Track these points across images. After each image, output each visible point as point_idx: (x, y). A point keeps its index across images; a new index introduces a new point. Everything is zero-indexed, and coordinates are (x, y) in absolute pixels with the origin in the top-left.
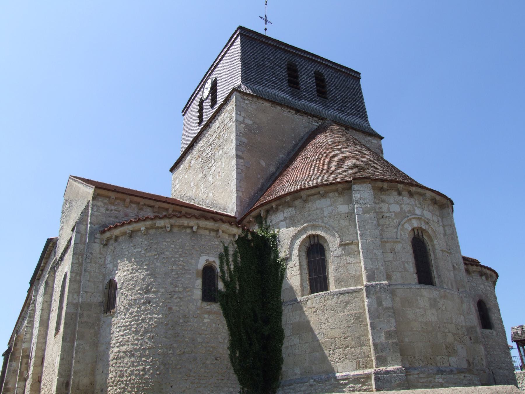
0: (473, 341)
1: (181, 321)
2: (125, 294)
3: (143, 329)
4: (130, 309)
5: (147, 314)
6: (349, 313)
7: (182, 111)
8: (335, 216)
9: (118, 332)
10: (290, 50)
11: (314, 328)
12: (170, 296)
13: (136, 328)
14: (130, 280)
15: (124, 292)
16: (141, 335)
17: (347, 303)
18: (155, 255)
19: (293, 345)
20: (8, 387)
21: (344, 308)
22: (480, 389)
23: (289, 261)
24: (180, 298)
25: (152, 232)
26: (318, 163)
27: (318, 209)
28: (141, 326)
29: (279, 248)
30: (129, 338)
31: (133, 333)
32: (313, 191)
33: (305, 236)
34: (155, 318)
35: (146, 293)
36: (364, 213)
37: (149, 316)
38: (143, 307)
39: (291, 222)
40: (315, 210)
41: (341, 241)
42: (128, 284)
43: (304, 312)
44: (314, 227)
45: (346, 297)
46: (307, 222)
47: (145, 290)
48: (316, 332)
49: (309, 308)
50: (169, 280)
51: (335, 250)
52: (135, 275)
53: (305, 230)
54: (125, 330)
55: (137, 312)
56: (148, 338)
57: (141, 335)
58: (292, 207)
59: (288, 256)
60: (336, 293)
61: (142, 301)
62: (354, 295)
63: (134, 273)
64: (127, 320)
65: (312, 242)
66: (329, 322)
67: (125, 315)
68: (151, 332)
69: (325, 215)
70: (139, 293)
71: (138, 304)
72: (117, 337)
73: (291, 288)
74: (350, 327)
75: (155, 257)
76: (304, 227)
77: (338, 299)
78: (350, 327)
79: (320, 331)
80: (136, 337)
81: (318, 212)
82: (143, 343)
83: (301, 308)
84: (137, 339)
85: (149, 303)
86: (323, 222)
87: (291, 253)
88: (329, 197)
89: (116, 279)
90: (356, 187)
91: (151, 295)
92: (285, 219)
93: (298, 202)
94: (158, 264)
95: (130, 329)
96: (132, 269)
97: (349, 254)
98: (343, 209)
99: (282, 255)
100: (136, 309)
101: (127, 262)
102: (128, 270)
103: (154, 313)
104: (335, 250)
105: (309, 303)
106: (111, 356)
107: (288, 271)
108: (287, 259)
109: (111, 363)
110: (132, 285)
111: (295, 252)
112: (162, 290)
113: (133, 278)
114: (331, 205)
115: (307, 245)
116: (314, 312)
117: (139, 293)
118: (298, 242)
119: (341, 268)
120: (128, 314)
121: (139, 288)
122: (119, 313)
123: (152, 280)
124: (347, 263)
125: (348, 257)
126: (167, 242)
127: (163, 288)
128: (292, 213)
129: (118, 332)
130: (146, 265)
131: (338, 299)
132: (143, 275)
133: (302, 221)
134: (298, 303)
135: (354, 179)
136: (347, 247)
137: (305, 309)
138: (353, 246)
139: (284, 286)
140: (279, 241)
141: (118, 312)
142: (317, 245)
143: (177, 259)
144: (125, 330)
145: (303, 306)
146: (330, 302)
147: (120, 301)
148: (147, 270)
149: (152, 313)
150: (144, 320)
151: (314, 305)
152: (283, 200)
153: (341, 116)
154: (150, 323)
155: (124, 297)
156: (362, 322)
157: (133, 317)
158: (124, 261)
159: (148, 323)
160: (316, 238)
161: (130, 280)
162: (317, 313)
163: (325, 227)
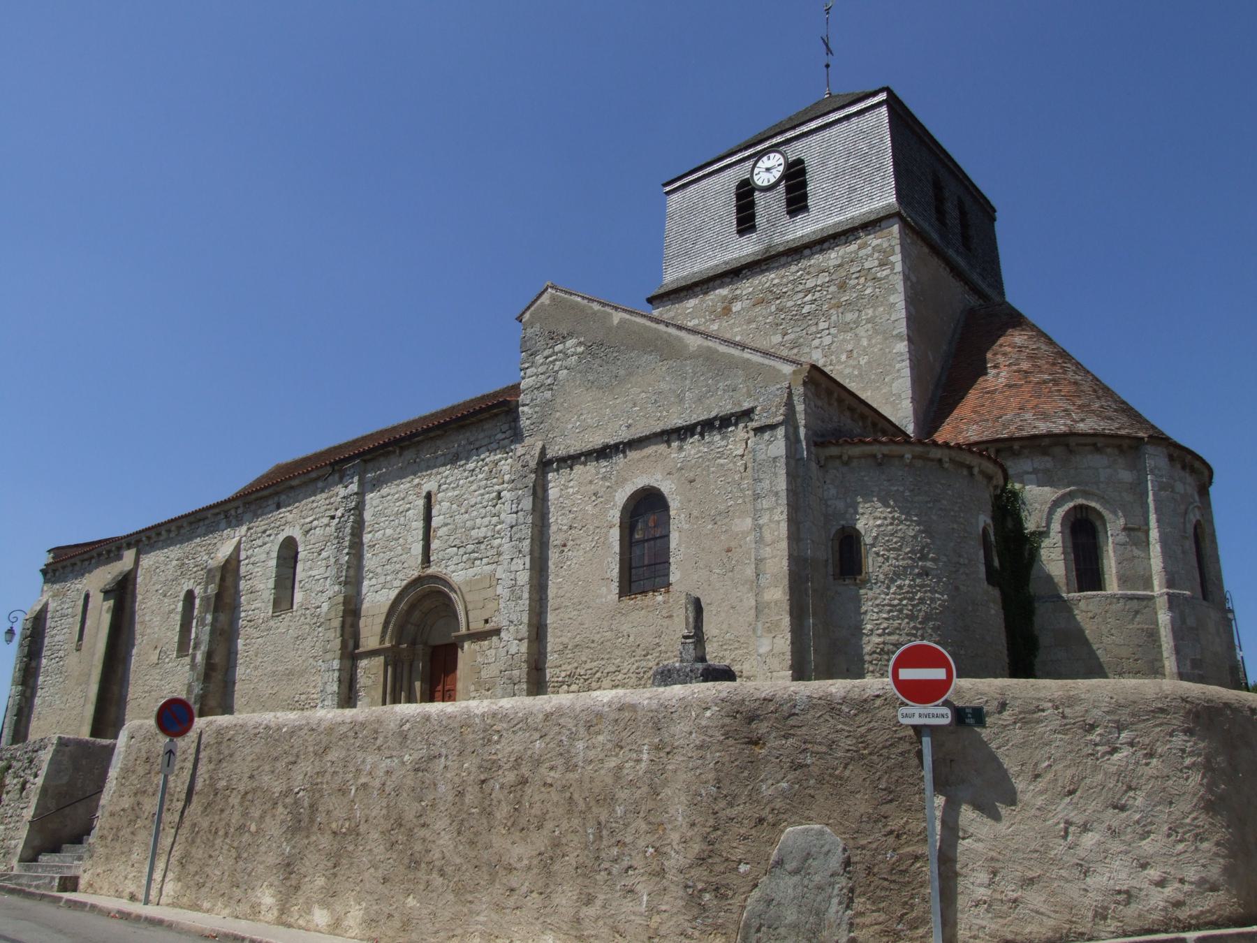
1: (970, 608)
2: (884, 555)
3: (922, 614)
4: (896, 581)
5: (926, 592)
6: (1138, 627)
7: (665, 182)
9: (877, 613)
10: (934, 148)
11: (1091, 641)
12: (954, 569)
13: (910, 610)
14: (892, 535)
15: (882, 553)
16: (920, 623)
17: (1137, 612)
18: (927, 502)
20: (212, 661)
21: (1133, 620)
23: (1045, 538)
24: (967, 574)
25: (919, 463)
26: (1060, 391)
28: (919, 608)
29: (1024, 514)
30: (900, 624)
31: (907, 618)
32: (1089, 440)
33: (1071, 504)
34: (939, 599)
35: (920, 559)
36: (1159, 490)
37: (929, 594)
38: (918, 581)
39: (1046, 479)
40: (1085, 469)
41: (1126, 524)
42: (888, 541)
43: (1074, 616)
44: (1086, 494)
45: (1135, 605)
46: (1073, 484)
47: (918, 555)
48: (1095, 647)
49: (1082, 611)
50: (952, 544)
51: (1118, 535)
52: (899, 528)
53: (1070, 496)
54: (889, 612)
55: (910, 586)
56: (931, 628)
57: (920, 623)
58: (1048, 455)
59: (1045, 529)
60: (1118, 598)
61: (917, 571)
62: (1145, 603)
63: (898, 525)
64: (893, 596)
65: (1079, 516)
66: (1112, 635)
67: (888, 588)
68: (935, 620)
69: (1102, 479)
70: (910, 558)
71: (910, 574)
72: (878, 620)
73: (1049, 579)
74: (1140, 646)
75: (929, 505)
76: (1071, 491)
77: (1125, 605)
78: (1140, 646)
79: (1101, 646)
80: (912, 624)
82: (925, 635)
83: (1070, 610)
84: (914, 628)
85: (927, 575)
86: (1098, 489)
87: (1048, 526)
89: (860, 526)
90: (1150, 449)
91: (929, 564)
92: (1035, 471)
94: (935, 518)
95: (901, 611)
96: (893, 518)
97: (1135, 544)
98: (1126, 476)
99: (1030, 525)
100: (907, 582)
101: (880, 505)
102: (885, 518)
103: (936, 592)
104: (1118, 535)
105: (1082, 604)
106: (867, 649)
107: (1044, 553)
108: (1043, 534)
109: (867, 658)
110: (896, 543)
111: (1056, 526)
112: (945, 559)
113: (896, 532)
114: (1109, 467)
115: (1072, 520)
116: (1091, 618)
117: (910, 558)
118: (1060, 512)
119: (1125, 563)
120: (893, 590)
121: (908, 549)
122: (876, 583)
123: (929, 540)
124: (1134, 557)
125: (1134, 548)
127: (945, 555)
129: (877, 613)
130: (916, 515)
131: (1125, 605)
132: (913, 530)
133: (1066, 481)
134: (1065, 601)
135: (1150, 437)
136: (1132, 533)
137: (1076, 612)
138: (1140, 534)
139: (1034, 572)
140: (1024, 503)
141: (873, 581)
144: (889, 612)
145: (1074, 607)
146: (1114, 607)
147: (873, 565)
148: (918, 524)
149: (933, 591)
150: (922, 601)
151: (1090, 607)
153: (980, 282)
154: (933, 606)
155: (881, 559)
156: (1155, 641)
157: (903, 593)
158: (873, 502)
159: (929, 605)
160: (1084, 510)
161: (892, 535)
162: (1095, 620)
163: (1103, 498)
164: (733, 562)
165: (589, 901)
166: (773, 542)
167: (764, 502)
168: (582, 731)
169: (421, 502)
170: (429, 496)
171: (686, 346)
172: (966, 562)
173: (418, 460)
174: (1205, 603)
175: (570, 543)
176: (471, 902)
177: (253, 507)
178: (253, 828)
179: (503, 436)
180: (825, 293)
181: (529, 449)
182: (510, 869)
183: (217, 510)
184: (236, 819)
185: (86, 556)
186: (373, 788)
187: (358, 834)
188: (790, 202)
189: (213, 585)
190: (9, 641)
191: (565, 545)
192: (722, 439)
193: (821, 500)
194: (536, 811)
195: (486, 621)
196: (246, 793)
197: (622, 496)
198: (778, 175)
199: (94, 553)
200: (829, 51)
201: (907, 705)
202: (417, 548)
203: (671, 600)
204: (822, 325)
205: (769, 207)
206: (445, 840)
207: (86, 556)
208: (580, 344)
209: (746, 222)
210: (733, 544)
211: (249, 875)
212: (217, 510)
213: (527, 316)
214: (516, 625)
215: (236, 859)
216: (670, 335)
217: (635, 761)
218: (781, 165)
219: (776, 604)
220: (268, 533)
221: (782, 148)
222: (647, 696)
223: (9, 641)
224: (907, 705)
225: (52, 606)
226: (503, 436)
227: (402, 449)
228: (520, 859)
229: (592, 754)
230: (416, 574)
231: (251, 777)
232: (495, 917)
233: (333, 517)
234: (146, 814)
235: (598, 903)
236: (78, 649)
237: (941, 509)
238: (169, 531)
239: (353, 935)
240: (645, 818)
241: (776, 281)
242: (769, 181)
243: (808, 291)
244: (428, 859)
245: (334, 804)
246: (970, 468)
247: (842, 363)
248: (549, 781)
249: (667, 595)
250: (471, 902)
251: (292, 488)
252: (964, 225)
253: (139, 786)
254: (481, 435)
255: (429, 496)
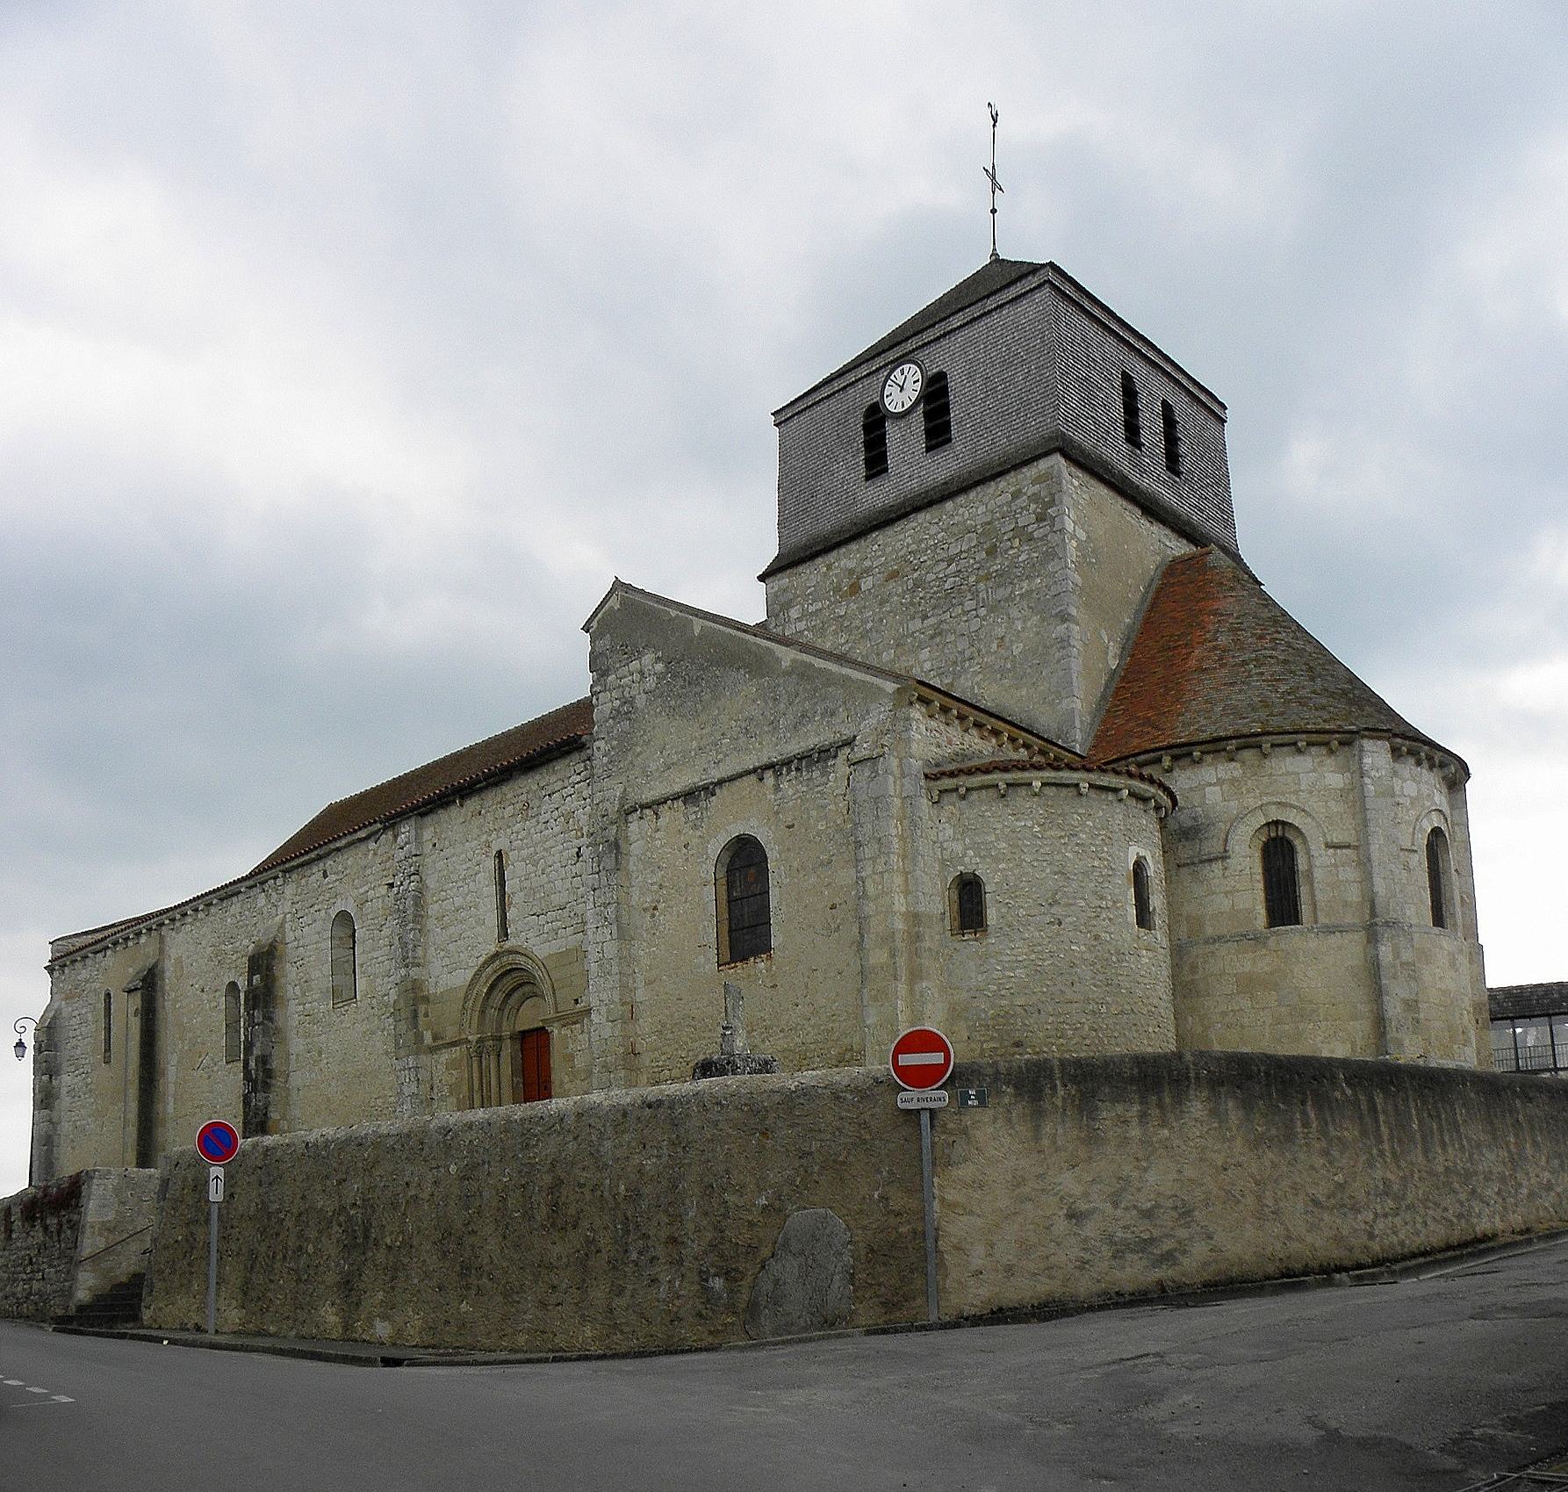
0: (1480, 1025)
8: (1320, 792)
18: (1061, 837)
19: (1238, 1011)
22: (402, 1372)
24: (1110, 919)
26: (1262, 674)
27: (1288, 773)
65: (1273, 835)
81: (1290, 779)
88: (1311, 755)
93: (1248, 754)
98: (1336, 780)
114: (1314, 771)
126: (1079, 815)
128: (1236, 774)
142: (1281, 838)
143: (1099, 849)
152: (1222, 744)
164: (838, 921)
165: (620, 1293)
166: (877, 897)
167: (866, 851)
168: (610, 1130)
169: (491, 863)
170: (499, 855)
171: (778, 660)
172: (1110, 903)
173: (483, 812)
174: (1437, 930)
175: (661, 906)
176: (518, 1302)
177: (294, 876)
178: (311, 1249)
179: (578, 778)
180: (971, 561)
181: (613, 791)
182: (551, 1267)
183: (251, 883)
184: (292, 1243)
185: (98, 947)
186: (422, 1199)
187: (411, 1246)
188: (930, 433)
189: (258, 976)
190: (20, 1056)
191: (655, 908)
192: (822, 775)
193: (934, 843)
194: (571, 1211)
195: (576, 1001)
196: (300, 1215)
197: (716, 847)
198: (914, 396)
199: (108, 943)
200: (996, 186)
201: (908, 1090)
202: (492, 920)
203: (774, 968)
204: (969, 605)
205: (904, 441)
206: (492, 1246)
207: (98, 947)
208: (658, 659)
209: (876, 463)
210: (837, 900)
211: (311, 1295)
212: (251, 883)
213: (594, 624)
214: (606, 1004)
215: (296, 1281)
216: (759, 646)
217: (657, 1157)
218: (918, 381)
219: (882, 968)
220: (316, 907)
221: (920, 355)
222: (688, 1087)
223: (20, 1056)
224: (908, 1090)
225: (66, 1011)
226: (578, 778)
227: (462, 798)
228: (559, 1258)
229: (618, 1153)
230: (493, 949)
231: (303, 1197)
232: (540, 1314)
233: (391, 885)
234: (201, 1244)
235: (628, 1293)
236: (107, 1062)
237: (1077, 844)
238: (196, 910)
239: (414, 1343)
240: (666, 1211)
241: (914, 547)
242: (903, 406)
243: (950, 561)
244: (477, 1265)
245: (386, 1219)
246: (1115, 790)
247: (992, 654)
248: (582, 1182)
249: (769, 963)
250: (518, 1302)
251: (338, 849)
252: (1171, 440)
253: (189, 1216)
254: (553, 778)
255: (499, 855)
